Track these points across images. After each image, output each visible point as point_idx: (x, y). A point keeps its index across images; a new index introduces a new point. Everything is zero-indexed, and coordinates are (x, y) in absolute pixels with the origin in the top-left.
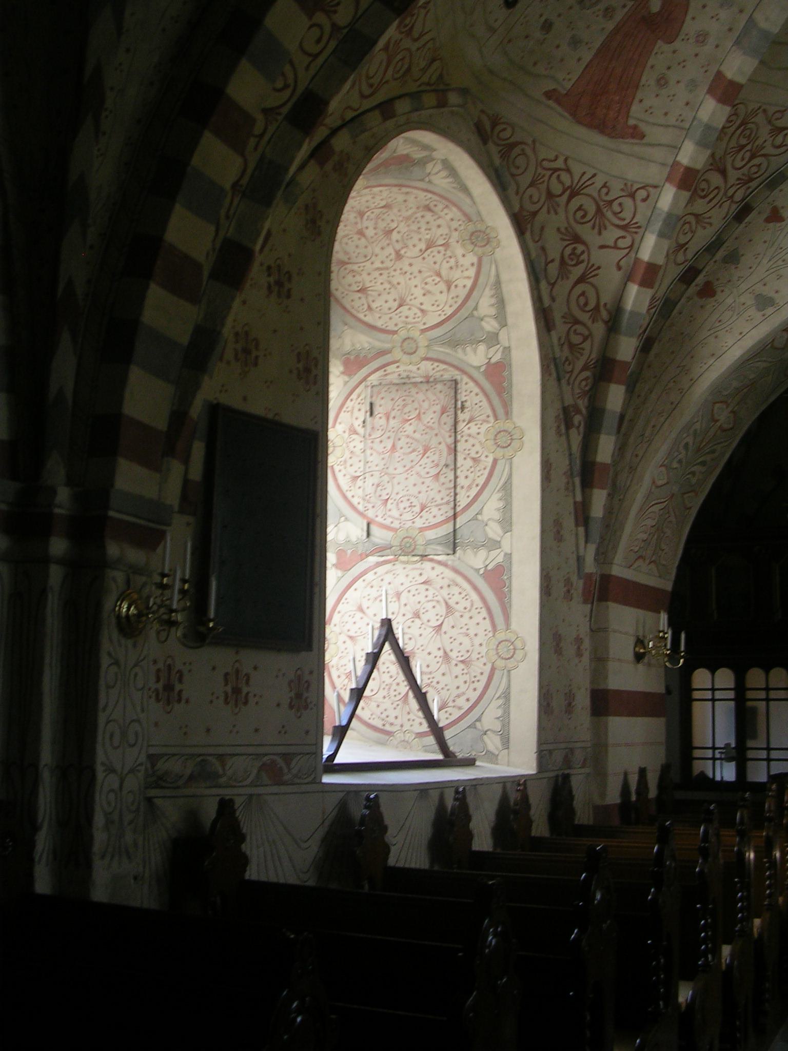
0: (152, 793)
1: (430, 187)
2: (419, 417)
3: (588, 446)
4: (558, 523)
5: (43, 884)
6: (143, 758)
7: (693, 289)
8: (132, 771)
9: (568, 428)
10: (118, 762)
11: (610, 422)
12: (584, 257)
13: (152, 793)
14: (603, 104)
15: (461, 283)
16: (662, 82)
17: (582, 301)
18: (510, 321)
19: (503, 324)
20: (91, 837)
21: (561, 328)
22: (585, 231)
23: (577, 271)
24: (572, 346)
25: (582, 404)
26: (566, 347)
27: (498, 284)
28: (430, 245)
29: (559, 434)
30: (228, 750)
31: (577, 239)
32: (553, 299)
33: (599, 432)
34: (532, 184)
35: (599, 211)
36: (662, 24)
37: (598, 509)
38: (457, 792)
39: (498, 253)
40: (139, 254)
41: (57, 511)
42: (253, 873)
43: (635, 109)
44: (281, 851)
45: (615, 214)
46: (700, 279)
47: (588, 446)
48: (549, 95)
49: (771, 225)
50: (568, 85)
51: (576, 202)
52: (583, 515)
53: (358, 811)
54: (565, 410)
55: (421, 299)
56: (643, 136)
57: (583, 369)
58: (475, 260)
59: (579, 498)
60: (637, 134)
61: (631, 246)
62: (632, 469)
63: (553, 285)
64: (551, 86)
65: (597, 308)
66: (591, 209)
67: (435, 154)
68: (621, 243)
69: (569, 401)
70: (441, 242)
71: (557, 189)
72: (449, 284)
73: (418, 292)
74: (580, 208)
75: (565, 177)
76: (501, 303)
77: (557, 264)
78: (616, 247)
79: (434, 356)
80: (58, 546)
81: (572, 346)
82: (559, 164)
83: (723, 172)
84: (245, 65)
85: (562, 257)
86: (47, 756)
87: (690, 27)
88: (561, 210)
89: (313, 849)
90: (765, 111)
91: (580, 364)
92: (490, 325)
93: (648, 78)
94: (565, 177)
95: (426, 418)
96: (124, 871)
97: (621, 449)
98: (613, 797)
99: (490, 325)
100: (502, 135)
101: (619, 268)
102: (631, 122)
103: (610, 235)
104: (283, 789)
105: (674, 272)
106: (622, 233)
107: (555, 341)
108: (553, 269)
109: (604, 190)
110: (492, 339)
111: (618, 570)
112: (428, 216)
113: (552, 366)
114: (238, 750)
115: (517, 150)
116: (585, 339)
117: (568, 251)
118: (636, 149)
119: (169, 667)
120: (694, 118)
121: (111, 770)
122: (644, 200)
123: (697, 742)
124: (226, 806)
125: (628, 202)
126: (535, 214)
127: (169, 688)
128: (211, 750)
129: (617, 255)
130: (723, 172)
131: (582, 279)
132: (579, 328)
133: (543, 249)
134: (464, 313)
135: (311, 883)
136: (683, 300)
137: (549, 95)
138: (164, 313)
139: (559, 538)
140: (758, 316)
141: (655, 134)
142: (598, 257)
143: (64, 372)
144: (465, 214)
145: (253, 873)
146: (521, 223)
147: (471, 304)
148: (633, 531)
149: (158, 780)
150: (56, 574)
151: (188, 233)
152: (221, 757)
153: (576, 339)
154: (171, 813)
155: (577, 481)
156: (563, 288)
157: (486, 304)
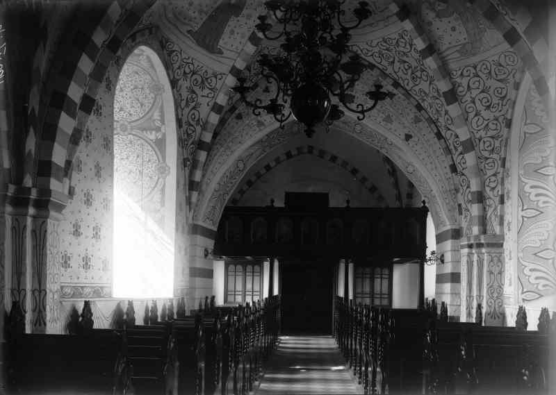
0: (61, 300)
1: (139, 65)
2: (127, 158)
3: (191, 174)
4: (181, 205)
5: (28, 331)
6: (59, 288)
7: (234, 115)
8: (56, 292)
9: (185, 166)
10: (52, 286)
11: (200, 165)
12: (196, 99)
13: (61, 300)
14: (208, 38)
15: (147, 105)
16: (232, 32)
17: (193, 117)
18: (166, 122)
19: (163, 123)
20: (46, 315)
21: (185, 127)
22: (196, 89)
23: (193, 104)
24: (188, 135)
25: (190, 157)
26: (186, 135)
27: (162, 107)
28: (136, 87)
29: (182, 169)
30: (84, 285)
31: (193, 92)
32: (182, 115)
33: (196, 168)
34: (179, 68)
35: (203, 82)
36: (236, 9)
37: (194, 199)
38: (129, 301)
39: (164, 95)
40: (59, 102)
41: (31, 197)
42: (96, 326)
43: (221, 42)
44: (102, 319)
45: (209, 83)
46: (237, 112)
47: (191, 174)
48: (189, 32)
49: (265, 94)
50: (196, 29)
51: (194, 77)
52: (189, 202)
53: (125, 308)
54: (184, 159)
55: (130, 109)
56: (222, 53)
57: (192, 143)
58: (153, 96)
59: (187, 194)
60: (220, 52)
61: (213, 97)
62: (208, 184)
63: (183, 109)
64: (189, 28)
65: (198, 120)
66: (200, 80)
67: (145, 54)
68: (210, 95)
69: (186, 157)
70: (140, 87)
71: (187, 70)
72: (142, 105)
73: (128, 106)
74: (196, 79)
75: (191, 66)
76: (162, 112)
77: (185, 101)
78: (207, 97)
79: (134, 133)
80: (31, 211)
81: (188, 135)
82: (190, 61)
83: (250, 71)
84: (99, 28)
85: (187, 98)
86: (29, 287)
87: (245, 12)
88: (188, 80)
89: (110, 320)
90: (268, 48)
91: (190, 142)
92: (158, 124)
93: (227, 30)
94: (191, 66)
95: (130, 159)
96: (55, 325)
97: (203, 176)
98: (197, 308)
99: (158, 124)
100: (170, 47)
101: (208, 105)
102: (219, 47)
103: (206, 91)
104: (101, 299)
105: (227, 108)
106: (210, 91)
107: (182, 132)
108: (183, 104)
109: (205, 74)
110: (158, 129)
111: (200, 223)
112: (137, 76)
113: (181, 142)
114: (87, 285)
115: (174, 54)
116: (193, 132)
117: (190, 96)
118: (220, 59)
119: (66, 255)
120: (243, 49)
121: (51, 291)
122: (220, 79)
123: (375, 292)
124: (87, 304)
125: (214, 79)
126: (178, 80)
127: (66, 262)
128: (78, 285)
129: (208, 100)
130: (250, 71)
131: (194, 108)
132: (192, 128)
133: (180, 94)
134: (147, 117)
135: (63, 333)
136: (230, 119)
137: (189, 32)
138: (66, 123)
139: (181, 210)
140: (258, 129)
141: (226, 53)
142: (200, 100)
143: (31, 144)
144: (152, 78)
145: (96, 326)
146: (174, 83)
147: (150, 114)
148: (204, 208)
149: (63, 296)
150: (29, 220)
151: (75, 92)
152: (82, 287)
153: (190, 132)
154: (68, 306)
155: (187, 187)
156: (187, 110)
157: (156, 115)
